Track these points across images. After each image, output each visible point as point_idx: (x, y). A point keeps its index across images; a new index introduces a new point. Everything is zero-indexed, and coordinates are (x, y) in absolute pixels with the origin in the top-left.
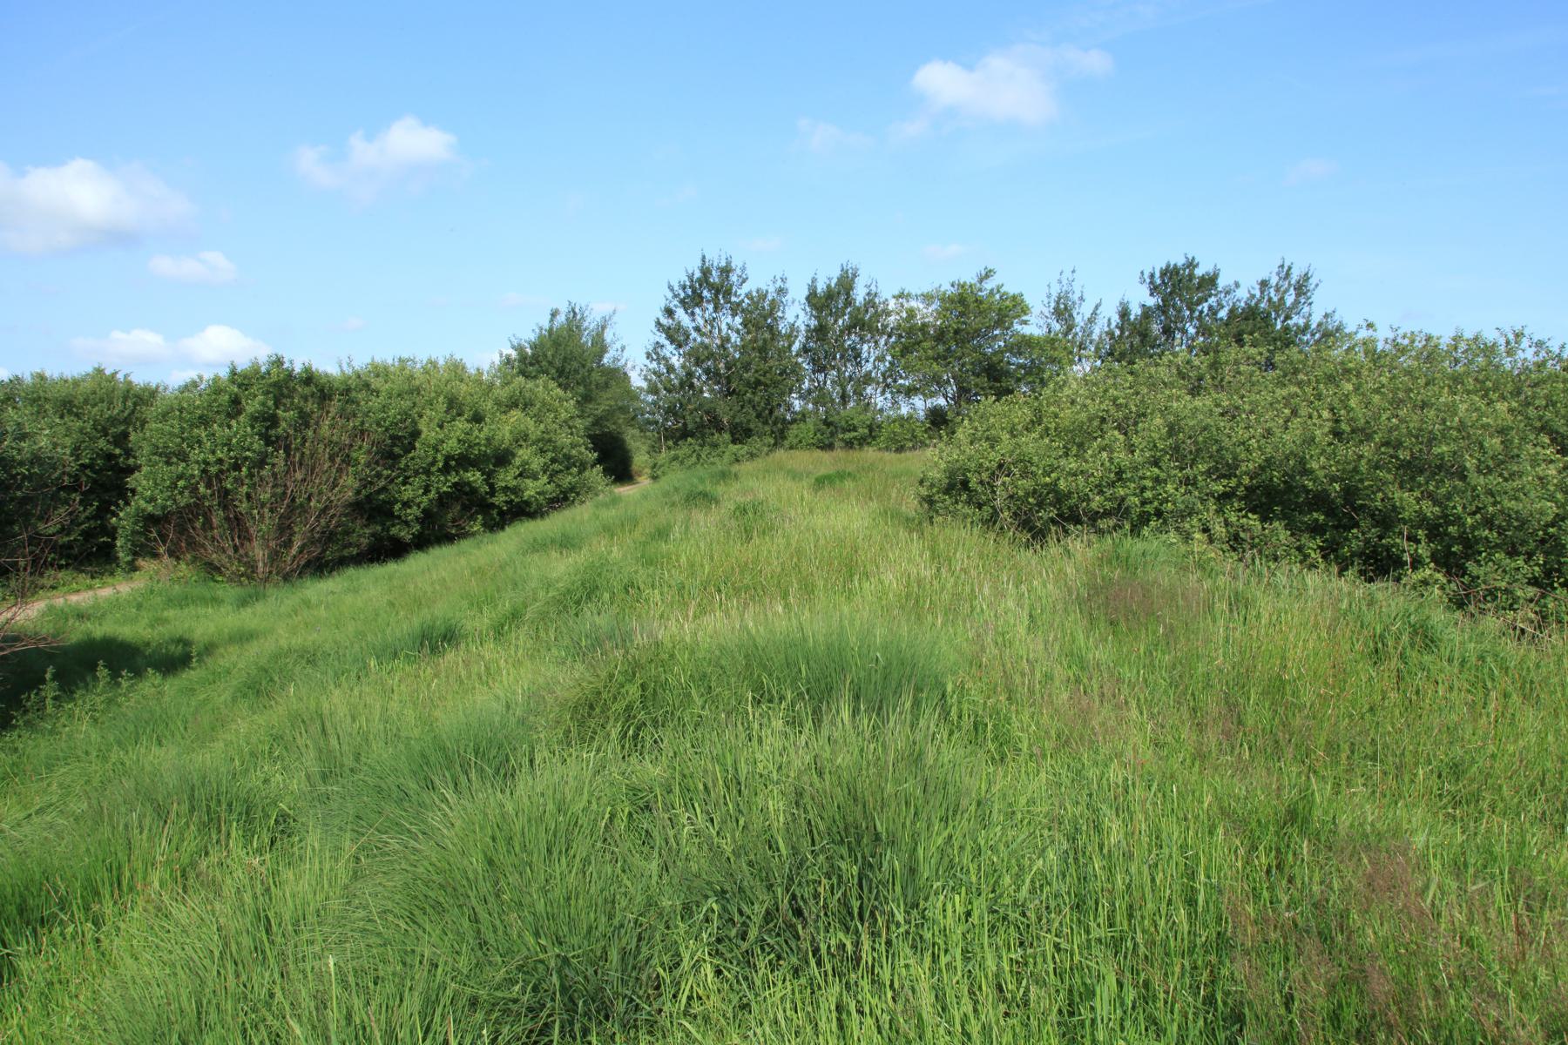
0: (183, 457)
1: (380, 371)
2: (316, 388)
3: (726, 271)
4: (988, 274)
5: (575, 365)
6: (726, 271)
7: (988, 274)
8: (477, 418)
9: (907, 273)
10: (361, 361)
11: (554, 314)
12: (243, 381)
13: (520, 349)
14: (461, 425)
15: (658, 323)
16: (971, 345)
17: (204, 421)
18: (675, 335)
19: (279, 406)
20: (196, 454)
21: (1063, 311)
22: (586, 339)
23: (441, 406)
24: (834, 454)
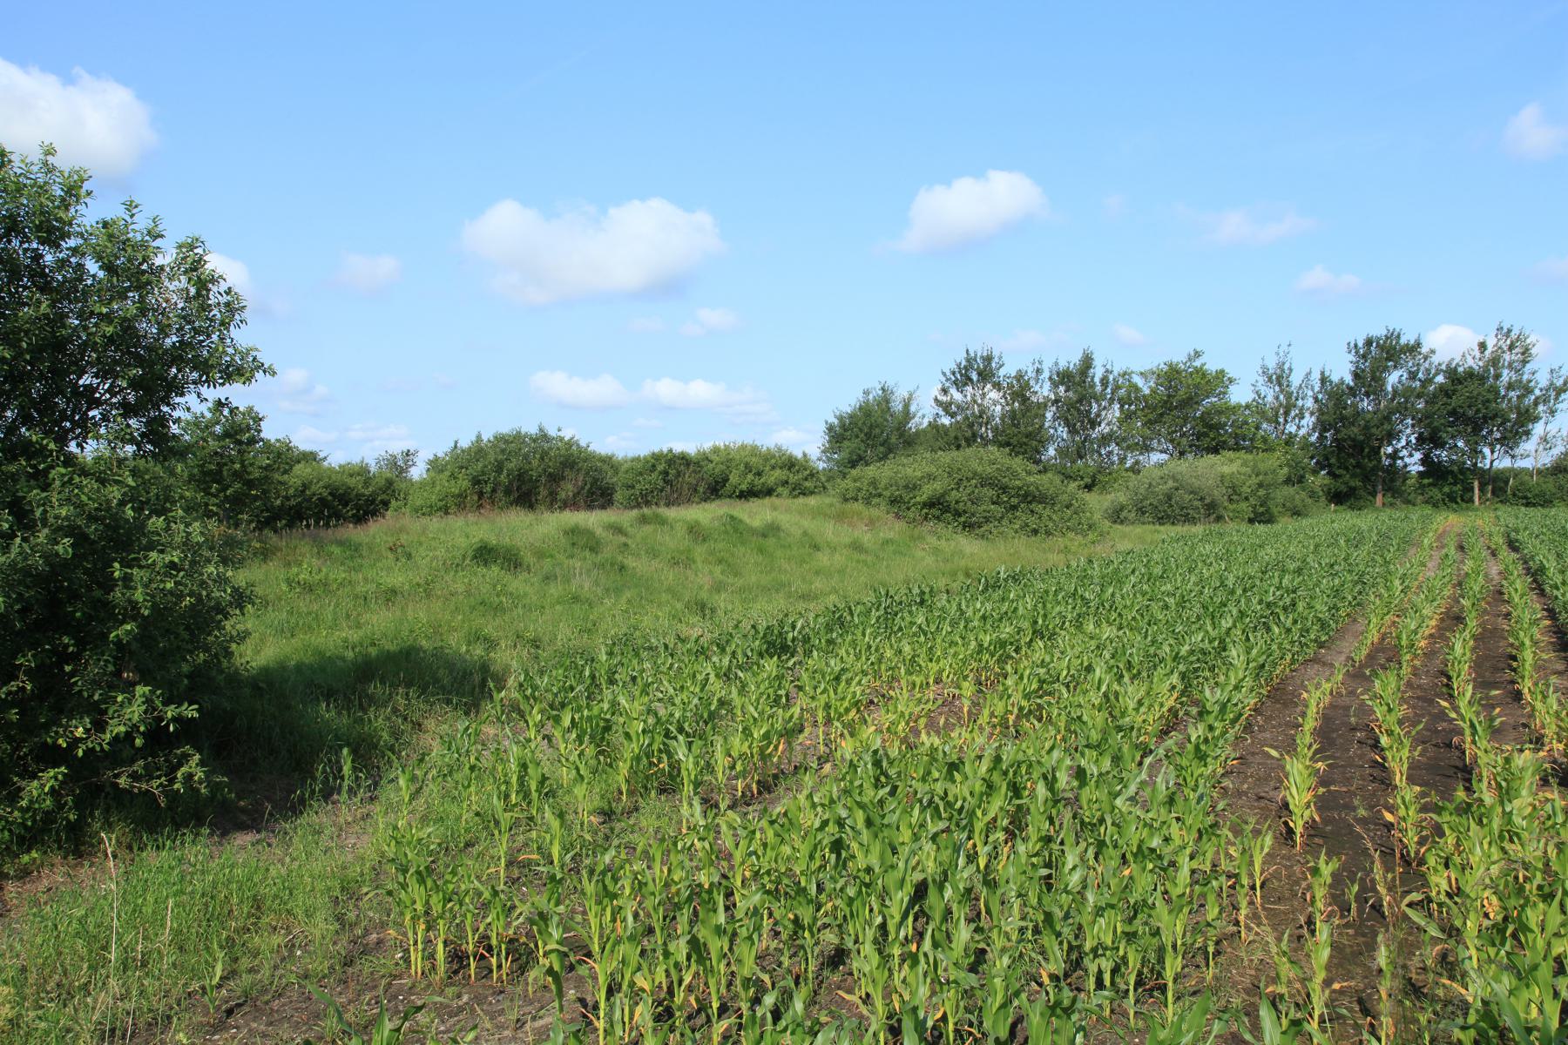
0: (633, 487)
1: (716, 450)
2: (684, 459)
3: (988, 359)
4: (1197, 354)
5: (877, 431)
6: (988, 359)
7: (1197, 354)
8: (759, 474)
9: (1133, 351)
10: (707, 446)
11: (866, 393)
12: (657, 457)
13: (841, 418)
14: (750, 477)
15: (936, 400)
16: (1184, 407)
17: (641, 474)
18: (946, 407)
19: (726, 458)
20: (638, 486)
21: (1279, 378)
22: (897, 406)
23: (742, 467)
24: (1277, 527)
